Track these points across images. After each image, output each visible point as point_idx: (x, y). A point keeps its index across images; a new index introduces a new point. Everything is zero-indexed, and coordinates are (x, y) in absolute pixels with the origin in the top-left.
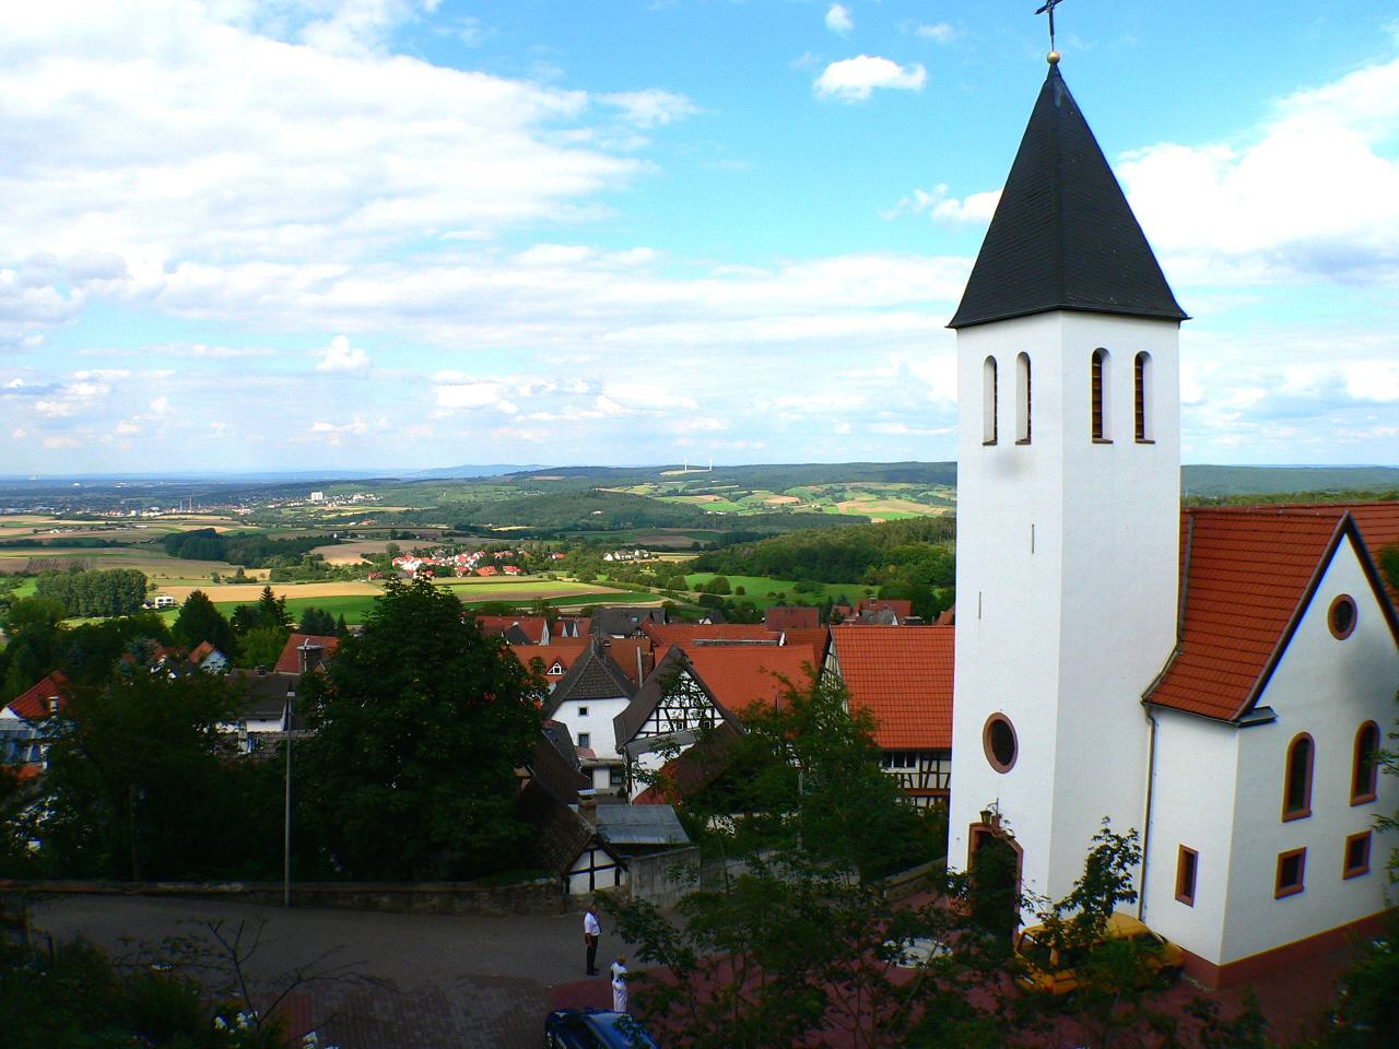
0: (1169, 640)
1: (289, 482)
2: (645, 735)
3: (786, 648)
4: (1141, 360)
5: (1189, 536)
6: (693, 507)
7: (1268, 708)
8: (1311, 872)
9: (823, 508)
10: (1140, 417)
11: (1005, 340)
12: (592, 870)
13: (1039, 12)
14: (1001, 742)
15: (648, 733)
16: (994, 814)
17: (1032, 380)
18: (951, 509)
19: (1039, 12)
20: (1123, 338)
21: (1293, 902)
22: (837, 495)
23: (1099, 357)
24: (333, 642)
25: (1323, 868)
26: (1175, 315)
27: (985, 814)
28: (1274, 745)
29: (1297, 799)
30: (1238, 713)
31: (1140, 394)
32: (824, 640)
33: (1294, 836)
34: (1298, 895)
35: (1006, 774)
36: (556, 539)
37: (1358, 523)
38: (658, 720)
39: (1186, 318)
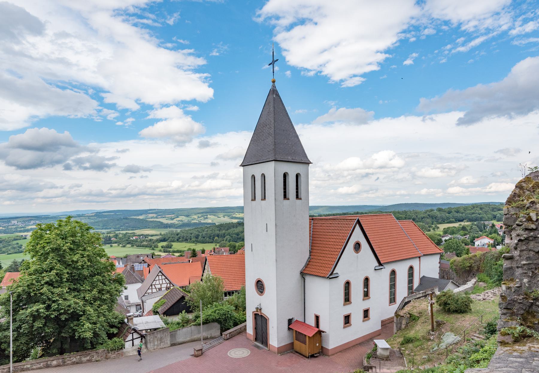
0: (307, 255)
1: (9, 217)
2: (148, 294)
3: (192, 263)
4: (297, 176)
5: (312, 226)
6: (159, 222)
7: (337, 273)
8: (353, 320)
9: (201, 221)
10: (297, 192)
11: (257, 170)
12: (133, 340)
13: (277, 60)
14: (260, 286)
15: (149, 293)
16: (259, 308)
17: (295, 191)
18: (242, 221)
19: (277, 60)
20: (292, 170)
21: (348, 329)
22: (205, 217)
23: (285, 175)
24: (51, 255)
25: (357, 318)
26: (307, 162)
27: (257, 308)
28: (340, 284)
29: (347, 299)
30: (329, 275)
31: (297, 186)
32: (205, 261)
33: (347, 310)
34: (349, 327)
35: (263, 296)
36: (112, 233)
37: (361, 221)
38: (152, 289)
39: (311, 163)
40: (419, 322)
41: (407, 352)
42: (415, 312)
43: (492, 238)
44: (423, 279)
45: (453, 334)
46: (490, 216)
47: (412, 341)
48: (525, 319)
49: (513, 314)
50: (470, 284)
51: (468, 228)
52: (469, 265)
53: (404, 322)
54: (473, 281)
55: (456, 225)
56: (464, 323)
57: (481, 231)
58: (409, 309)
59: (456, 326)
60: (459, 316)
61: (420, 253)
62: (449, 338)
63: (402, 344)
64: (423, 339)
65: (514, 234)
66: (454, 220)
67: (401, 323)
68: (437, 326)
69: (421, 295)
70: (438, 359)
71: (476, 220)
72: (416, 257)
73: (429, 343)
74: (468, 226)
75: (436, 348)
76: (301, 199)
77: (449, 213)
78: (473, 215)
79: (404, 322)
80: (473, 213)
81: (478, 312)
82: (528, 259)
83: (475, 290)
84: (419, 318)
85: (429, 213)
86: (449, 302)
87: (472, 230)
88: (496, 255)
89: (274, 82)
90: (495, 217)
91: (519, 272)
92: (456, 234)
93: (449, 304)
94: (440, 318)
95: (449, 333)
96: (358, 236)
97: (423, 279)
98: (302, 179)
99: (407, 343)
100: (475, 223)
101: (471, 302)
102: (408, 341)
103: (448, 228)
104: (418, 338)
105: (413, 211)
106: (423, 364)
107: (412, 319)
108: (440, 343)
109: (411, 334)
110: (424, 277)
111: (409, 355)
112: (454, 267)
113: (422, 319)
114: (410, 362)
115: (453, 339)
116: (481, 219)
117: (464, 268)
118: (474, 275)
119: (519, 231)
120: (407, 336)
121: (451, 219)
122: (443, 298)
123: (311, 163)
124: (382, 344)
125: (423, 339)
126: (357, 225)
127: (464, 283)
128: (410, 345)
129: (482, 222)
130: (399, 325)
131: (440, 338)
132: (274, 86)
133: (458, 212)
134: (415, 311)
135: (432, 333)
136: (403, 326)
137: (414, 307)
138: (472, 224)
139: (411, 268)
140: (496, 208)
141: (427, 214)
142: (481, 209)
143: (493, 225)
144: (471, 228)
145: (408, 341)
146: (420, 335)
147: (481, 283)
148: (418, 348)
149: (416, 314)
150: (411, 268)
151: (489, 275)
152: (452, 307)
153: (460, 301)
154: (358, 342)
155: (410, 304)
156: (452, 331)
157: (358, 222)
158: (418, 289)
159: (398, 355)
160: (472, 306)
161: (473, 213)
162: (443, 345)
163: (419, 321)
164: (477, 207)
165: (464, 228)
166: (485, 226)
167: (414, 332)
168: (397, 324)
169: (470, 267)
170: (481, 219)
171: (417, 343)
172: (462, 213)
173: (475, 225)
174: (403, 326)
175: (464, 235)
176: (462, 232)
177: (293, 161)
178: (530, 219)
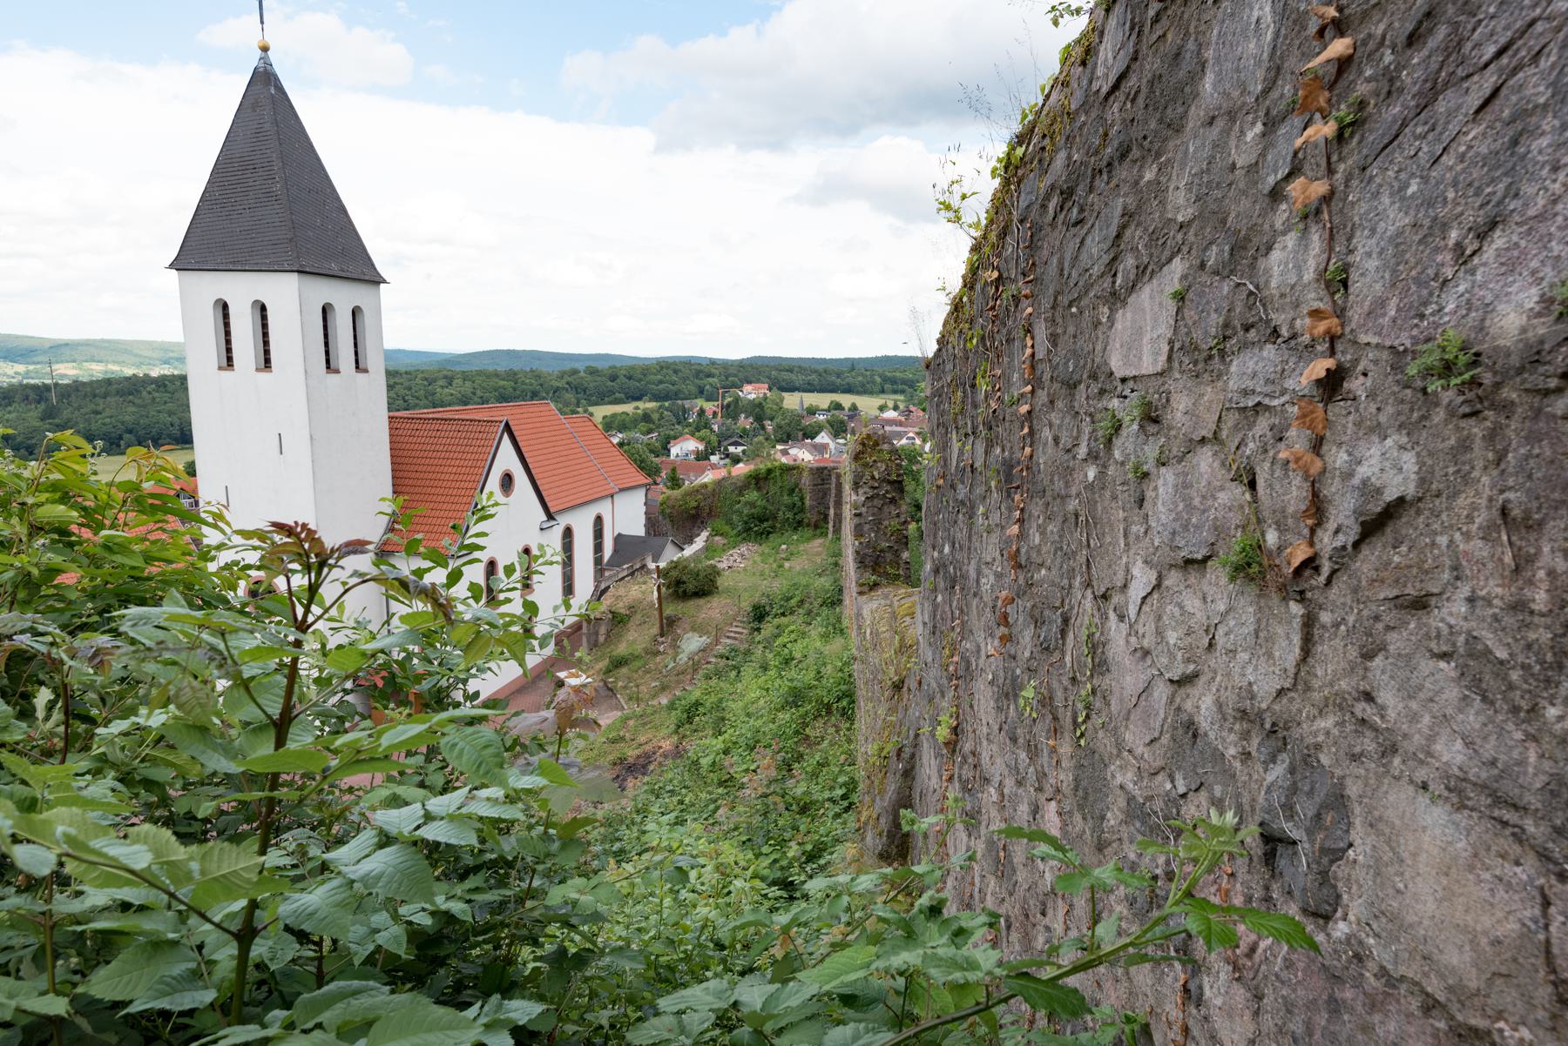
4: (356, 312)
20: (343, 297)
23: (326, 311)
26: (377, 279)
39: (384, 282)
40: (632, 624)
41: (620, 684)
42: (621, 608)
43: (701, 439)
44: (619, 539)
45: (696, 635)
46: (692, 388)
47: (626, 663)
48: (874, 570)
49: (865, 567)
50: (699, 542)
51: (655, 416)
52: (695, 504)
53: (603, 630)
54: (705, 534)
55: (628, 408)
56: (710, 612)
57: (679, 423)
58: (608, 602)
59: (699, 621)
60: (701, 601)
61: (613, 486)
62: (692, 643)
63: (608, 671)
64: (647, 653)
65: (861, 491)
66: (623, 396)
67: (597, 634)
68: (668, 625)
69: (625, 573)
70: (678, 682)
71: (666, 398)
72: (607, 496)
73: (658, 659)
74: (652, 410)
75: (672, 665)
76: (366, 371)
77: (613, 378)
78: (661, 387)
79: (603, 630)
80: (661, 382)
81: (727, 590)
82: (873, 515)
83: (708, 549)
84: (629, 617)
85: (569, 379)
86: (684, 578)
87: (662, 422)
88: (739, 484)
89: (265, 49)
90: (701, 392)
91: (867, 527)
92: (630, 430)
93: (684, 583)
94: (669, 610)
95: (690, 635)
96: (507, 458)
97: (619, 539)
98: (367, 319)
99: (617, 667)
100: (667, 404)
101: (718, 573)
102: (619, 663)
103: (614, 416)
104: (636, 653)
105: (532, 371)
106: (654, 697)
107: (618, 621)
108: (677, 654)
109: (622, 649)
110: (619, 535)
111: (625, 687)
112: (668, 511)
113: (638, 618)
114: (630, 699)
115: (699, 644)
116: (676, 395)
117: (687, 510)
118: (703, 525)
119: (867, 489)
120: (614, 653)
121: (617, 395)
122: (674, 573)
123: (384, 282)
124: (574, 679)
125: (647, 653)
126: (506, 435)
127: (690, 541)
128: (624, 670)
129: (680, 402)
130: (593, 638)
131: (675, 646)
132: (265, 60)
133: (630, 378)
134: (621, 605)
135: (660, 640)
136: (602, 639)
137: (618, 598)
138: (660, 407)
139: (599, 520)
140: (701, 371)
141: (564, 381)
142: (676, 372)
143: (702, 412)
144: (661, 417)
145: (619, 663)
146: (639, 648)
147: (717, 538)
148: (640, 672)
149: (623, 611)
150: (599, 520)
151: (729, 522)
152: (691, 587)
153: (702, 574)
154: (514, 688)
155: (608, 594)
156: (693, 629)
157: (508, 428)
158: (612, 563)
159: (604, 692)
160: (720, 582)
161: (661, 382)
162: (683, 658)
163: (631, 624)
164: (667, 368)
165: (646, 417)
166: (684, 411)
167: (624, 644)
168: (589, 636)
169: (697, 508)
170: (676, 395)
171: (637, 664)
172: (639, 381)
173: (667, 409)
174: (602, 639)
175: (649, 433)
176: (643, 426)
177: (343, 274)
178: (873, 477)
